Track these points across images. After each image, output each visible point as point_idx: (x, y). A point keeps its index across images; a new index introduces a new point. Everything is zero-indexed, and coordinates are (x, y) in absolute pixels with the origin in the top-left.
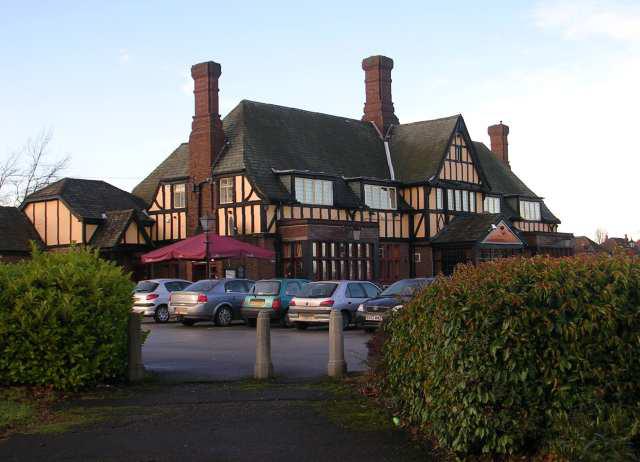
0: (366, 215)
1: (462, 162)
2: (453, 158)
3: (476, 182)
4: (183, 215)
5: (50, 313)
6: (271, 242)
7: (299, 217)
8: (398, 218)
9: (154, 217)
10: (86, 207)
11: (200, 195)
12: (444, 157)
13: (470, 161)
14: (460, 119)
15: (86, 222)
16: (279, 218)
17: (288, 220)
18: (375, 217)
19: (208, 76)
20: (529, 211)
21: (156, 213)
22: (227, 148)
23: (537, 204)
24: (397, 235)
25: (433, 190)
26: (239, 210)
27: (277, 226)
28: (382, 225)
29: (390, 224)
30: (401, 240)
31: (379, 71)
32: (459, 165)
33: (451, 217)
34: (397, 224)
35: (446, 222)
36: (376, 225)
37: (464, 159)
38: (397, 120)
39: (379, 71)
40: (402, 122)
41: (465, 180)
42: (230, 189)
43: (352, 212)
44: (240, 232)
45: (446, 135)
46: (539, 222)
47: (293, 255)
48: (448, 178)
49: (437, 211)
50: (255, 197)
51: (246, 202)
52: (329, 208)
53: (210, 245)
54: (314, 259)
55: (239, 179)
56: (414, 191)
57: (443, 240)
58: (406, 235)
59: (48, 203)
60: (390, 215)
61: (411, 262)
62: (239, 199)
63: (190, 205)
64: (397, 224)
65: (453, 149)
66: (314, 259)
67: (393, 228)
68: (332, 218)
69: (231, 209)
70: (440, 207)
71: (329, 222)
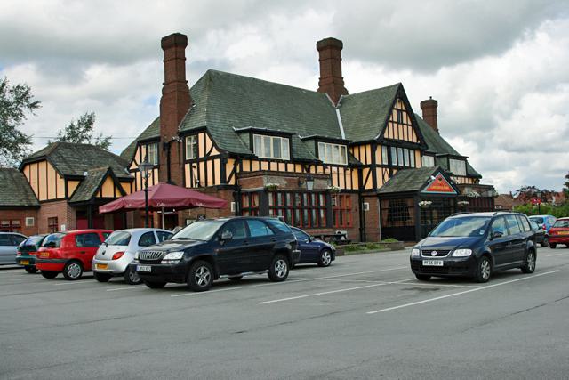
0: (320, 169)
1: (403, 124)
2: (395, 120)
3: (415, 141)
4: (156, 171)
5: (487, 200)
6: (230, 193)
7: (258, 169)
8: (348, 172)
9: (133, 174)
10: (70, 167)
11: (169, 153)
12: (388, 117)
13: (410, 123)
14: (400, 87)
15: (67, 178)
16: (238, 171)
17: (246, 172)
18: (328, 171)
19: (175, 46)
20: (457, 168)
21: (135, 171)
22: (193, 110)
23: (463, 163)
24: (349, 187)
25: (379, 148)
26: (202, 164)
27: (236, 178)
28: (334, 177)
29: (342, 177)
30: (352, 191)
31: (330, 51)
32: (400, 126)
33: (395, 171)
34: (348, 178)
35: (391, 176)
36: (329, 177)
37: (405, 122)
38: (345, 92)
39: (330, 51)
40: (351, 92)
41: (406, 139)
42: (194, 145)
43: (307, 166)
44: (203, 185)
45: (389, 100)
46: (465, 177)
47: (251, 205)
48: (391, 137)
49: (382, 166)
50: (215, 152)
51: (208, 157)
52: (286, 162)
53: (149, 192)
54: (271, 208)
55: (201, 136)
56: (362, 149)
57: (390, 190)
58: (356, 187)
59: (40, 164)
60: (341, 170)
61: (360, 211)
62: (202, 155)
63: (161, 163)
64: (348, 178)
65: (395, 112)
66: (271, 208)
67: (343, 181)
68: (289, 170)
69: (195, 164)
70: (385, 163)
71: (286, 173)
